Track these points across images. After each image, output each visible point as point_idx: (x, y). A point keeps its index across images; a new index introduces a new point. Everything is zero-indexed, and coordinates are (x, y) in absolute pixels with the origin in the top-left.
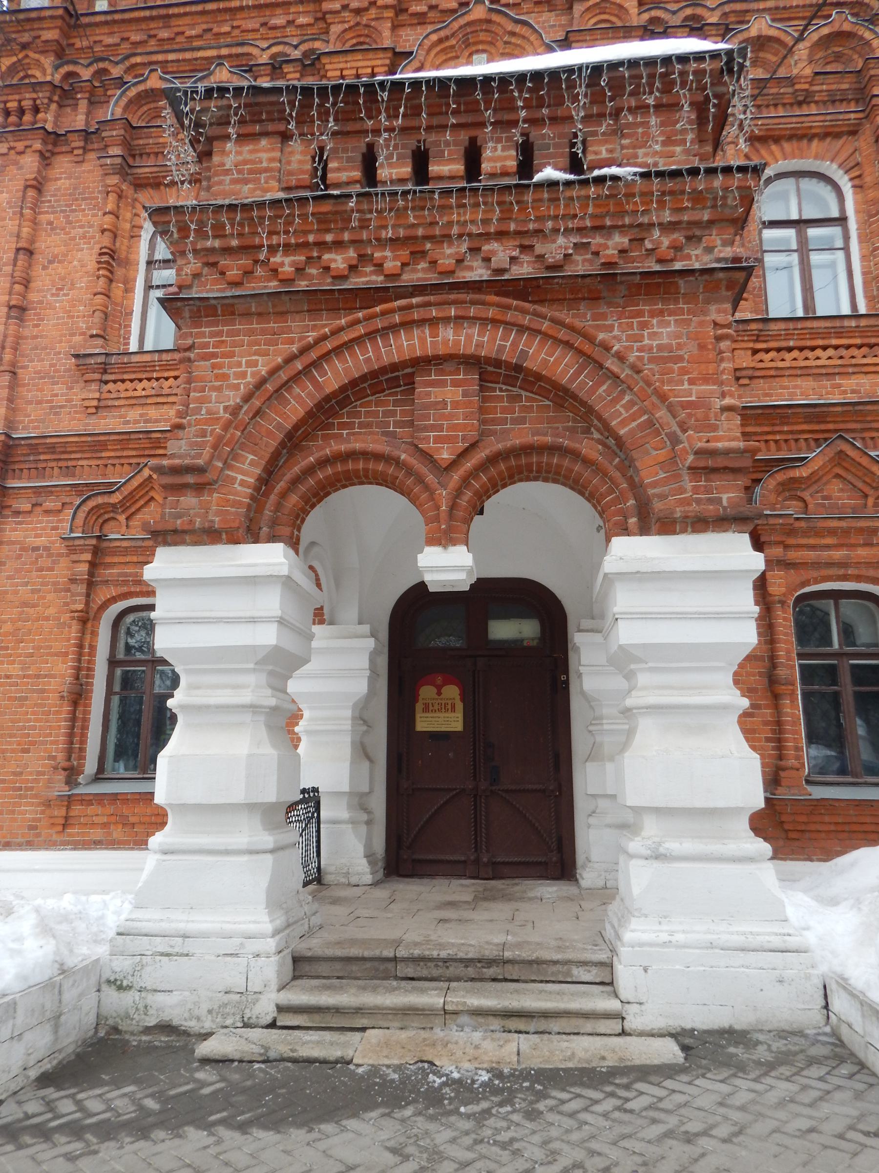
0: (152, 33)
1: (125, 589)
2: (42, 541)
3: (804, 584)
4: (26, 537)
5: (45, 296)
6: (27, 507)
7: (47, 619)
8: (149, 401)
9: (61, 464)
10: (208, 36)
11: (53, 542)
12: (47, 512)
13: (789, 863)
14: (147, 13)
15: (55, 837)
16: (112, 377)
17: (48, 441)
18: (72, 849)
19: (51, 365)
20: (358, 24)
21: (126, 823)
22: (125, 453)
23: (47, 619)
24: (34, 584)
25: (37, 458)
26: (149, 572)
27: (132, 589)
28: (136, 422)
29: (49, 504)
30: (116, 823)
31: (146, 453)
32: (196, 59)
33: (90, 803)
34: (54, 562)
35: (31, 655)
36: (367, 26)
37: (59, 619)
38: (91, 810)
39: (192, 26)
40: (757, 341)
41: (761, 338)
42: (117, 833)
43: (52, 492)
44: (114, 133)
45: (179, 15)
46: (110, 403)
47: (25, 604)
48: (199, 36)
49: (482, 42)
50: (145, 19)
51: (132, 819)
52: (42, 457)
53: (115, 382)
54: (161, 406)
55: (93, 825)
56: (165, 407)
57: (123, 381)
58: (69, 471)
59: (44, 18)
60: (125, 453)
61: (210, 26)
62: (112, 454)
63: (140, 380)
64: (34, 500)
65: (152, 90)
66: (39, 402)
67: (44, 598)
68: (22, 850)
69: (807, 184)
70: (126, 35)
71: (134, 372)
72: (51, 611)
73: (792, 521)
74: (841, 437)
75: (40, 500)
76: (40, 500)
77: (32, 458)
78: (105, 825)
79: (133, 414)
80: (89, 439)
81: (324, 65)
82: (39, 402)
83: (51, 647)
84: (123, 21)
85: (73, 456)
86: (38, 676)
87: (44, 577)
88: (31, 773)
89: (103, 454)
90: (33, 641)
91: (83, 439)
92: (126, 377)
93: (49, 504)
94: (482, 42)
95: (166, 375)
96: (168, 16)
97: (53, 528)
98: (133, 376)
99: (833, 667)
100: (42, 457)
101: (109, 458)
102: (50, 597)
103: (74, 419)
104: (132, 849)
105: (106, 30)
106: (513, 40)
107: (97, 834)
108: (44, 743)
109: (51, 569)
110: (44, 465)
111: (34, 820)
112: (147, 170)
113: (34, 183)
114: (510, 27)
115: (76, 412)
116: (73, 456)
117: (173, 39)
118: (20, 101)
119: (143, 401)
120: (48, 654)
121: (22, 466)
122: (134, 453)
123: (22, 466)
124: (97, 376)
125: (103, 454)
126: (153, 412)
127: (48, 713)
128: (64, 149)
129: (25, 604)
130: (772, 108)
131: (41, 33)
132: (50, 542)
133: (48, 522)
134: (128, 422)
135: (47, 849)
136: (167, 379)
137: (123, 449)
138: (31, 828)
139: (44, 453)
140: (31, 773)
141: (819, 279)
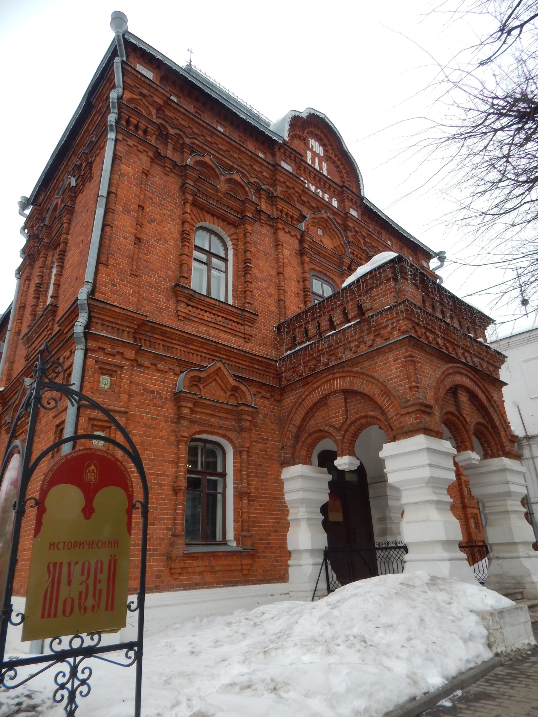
0: (204, 134)
1: (203, 428)
2: (155, 387)
3: (200, 432)
4: (146, 383)
5: (151, 239)
6: (148, 364)
7: (161, 438)
8: (210, 324)
9: (165, 343)
10: (227, 153)
11: (163, 390)
12: (159, 370)
13: (250, 586)
14: (206, 125)
15: (173, 582)
16: (192, 304)
17: (165, 328)
18: (183, 590)
19: (156, 282)
20: (287, 191)
21: (214, 572)
22: (201, 349)
23: (161, 438)
24: (153, 414)
25: (152, 335)
26: (382, 454)
27: (207, 429)
28: (203, 334)
29: (161, 366)
30: (206, 572)
31: (211, 353)
32: (222, 160)
33: (197, 558)
34: (163, 402)
35: (153, 460)
36: (289, 194)
37: (168, 439)
38: (196, 563)
39: (222, 145)
40: (190, 300)
41: (192, 300)
42: (208, 577)
43: (164, 359)
44: (193, 175)
45: (217, 135)
46: (191, 318)
47: (147, 426)
48: (224, 151)
49: (321, 225)
50: (204, 126)
51: (217, 568)
52: (155, 336)
53: (222, 317)
54: (215, 330)
55: (194, 573)
56: (217, 331)
57: (197, 308)
58: (167, 348)
59: (159, 91)
60: (201, 349)
61: (229, 150)
62: (194, 348)
63: (206, 311)
64: (153, 362)
65: (206, 163)
66: (150, 301)
67: (159, 424)
68: (153, 592)
69: (214, 239)
70: (191, 126)
71: (203, 306)
72: (164, 434)
73: (197, 398)
74: (220, 360)
75: (156, 362)
76: (156, 362)
77: (149, 334)
78: (201, 573)
79: (202, 329)
80: (187, 336)
81: (277, 201)
82: (150, 301)
83: (164, 456)
84: (193, 120)
85: (173, 341)
86: (158, 475)
87: (158, 411)
88: (156, 539)
89: (190, 346)
90: (154, 451)
91: (184, 334)
92: (199, 306)
93: (161, 366)
94: (321, 225)
95: (219, 314)
96: (214, 133)
97: (162, 382)
98: (203, 308)
99: (199, 479)
100: (155, 336)
101: (191, 349)
102: (163, 424)
103: (171, 319)
104: (216, 587)
105: (182, 116)
106: (333, 232)
107: (197, 579)
108: (163, 519)
109: (162, 407)
110: (155, 341)
111: (159, 571)
112: (202, 200)
113: (147, 172)
114: (334, 228)
115: (172, 316)
116: (173, 341)
117: (173, 119)
118: (138, 122)
119: (207, 323)
120: (163, 461)
121: (141, 337)
122: (205, 351)
123: (141, 337)
124: (185, 300)
125: (190, 346)
126: (211, 331)
127: (164, 499)
128: (159, 162)
129: (147, 426)
130: (229, 209)
131: (154, 96)
132: (160, 389)
133: (159, 377)
134: (199, 332)
135: (168, 591)
136: (219, 316)
137: (200, 347)
138: (158, 577)
139: (157, 334)
140: (156, 539)
141: (213, 282)
